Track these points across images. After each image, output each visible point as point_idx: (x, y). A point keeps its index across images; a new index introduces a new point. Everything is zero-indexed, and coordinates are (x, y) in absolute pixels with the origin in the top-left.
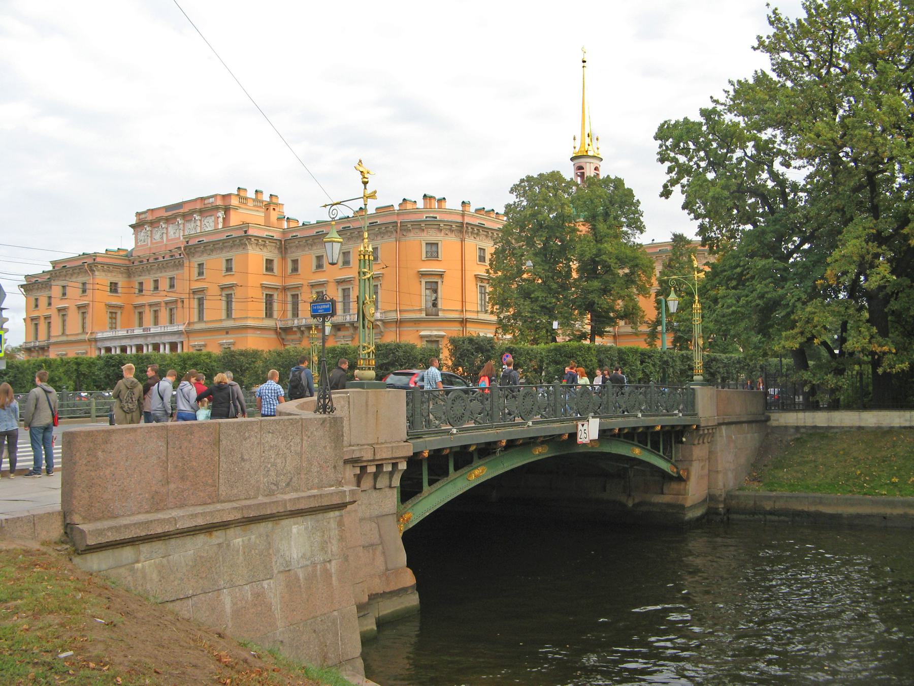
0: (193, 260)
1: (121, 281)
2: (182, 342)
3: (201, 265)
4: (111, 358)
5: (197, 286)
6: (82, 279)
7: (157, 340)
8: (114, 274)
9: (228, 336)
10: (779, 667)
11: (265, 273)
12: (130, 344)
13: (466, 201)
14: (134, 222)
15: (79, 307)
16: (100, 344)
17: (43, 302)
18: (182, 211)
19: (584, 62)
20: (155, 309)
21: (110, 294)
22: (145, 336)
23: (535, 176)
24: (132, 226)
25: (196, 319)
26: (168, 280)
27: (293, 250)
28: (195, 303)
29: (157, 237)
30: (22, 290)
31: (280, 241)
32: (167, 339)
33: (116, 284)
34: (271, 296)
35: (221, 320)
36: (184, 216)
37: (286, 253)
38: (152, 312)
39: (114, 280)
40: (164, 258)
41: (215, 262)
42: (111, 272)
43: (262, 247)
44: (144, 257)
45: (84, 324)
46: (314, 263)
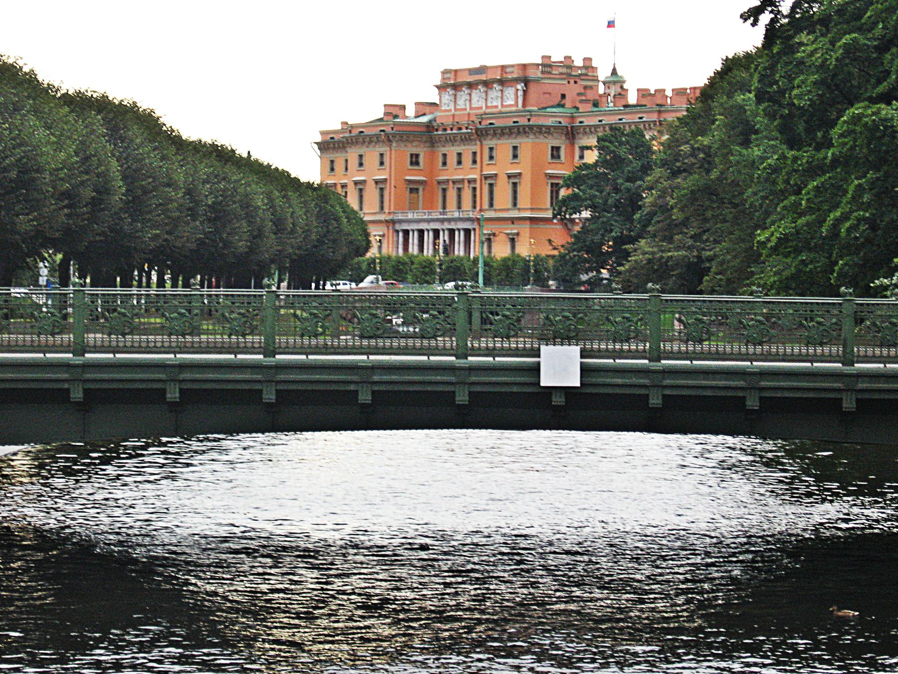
0: (485, 143)
1: (422, 151)
2: (474, 229)
3: (491, 149)
4: (452, 261)
7: (452, 226)
8: (414, 144)
9: (513, 226)
11: (550, 161)
12: (428, 227)
14: (439, 83)
15: (377, 182)
16: (398, 227)
17: (339, 166)
18: (483, 77)
20: (381, 186)
22: (442, 221)
23: (292, 176)
24: (437, 87)
25: (486, 205)
26: (511, 149)
27: (580, 136)
29: (461, 103)
30: (316, 147)
31: (567, 127)
32: (447, 226)
35: (508, 210)
36: (487, 84)
38: (511, 185)
39: (415, 151)
41: (504, 147)
42: (411, 142)
43: (546, 135)
44: (448, 125)
45: (382, 202)
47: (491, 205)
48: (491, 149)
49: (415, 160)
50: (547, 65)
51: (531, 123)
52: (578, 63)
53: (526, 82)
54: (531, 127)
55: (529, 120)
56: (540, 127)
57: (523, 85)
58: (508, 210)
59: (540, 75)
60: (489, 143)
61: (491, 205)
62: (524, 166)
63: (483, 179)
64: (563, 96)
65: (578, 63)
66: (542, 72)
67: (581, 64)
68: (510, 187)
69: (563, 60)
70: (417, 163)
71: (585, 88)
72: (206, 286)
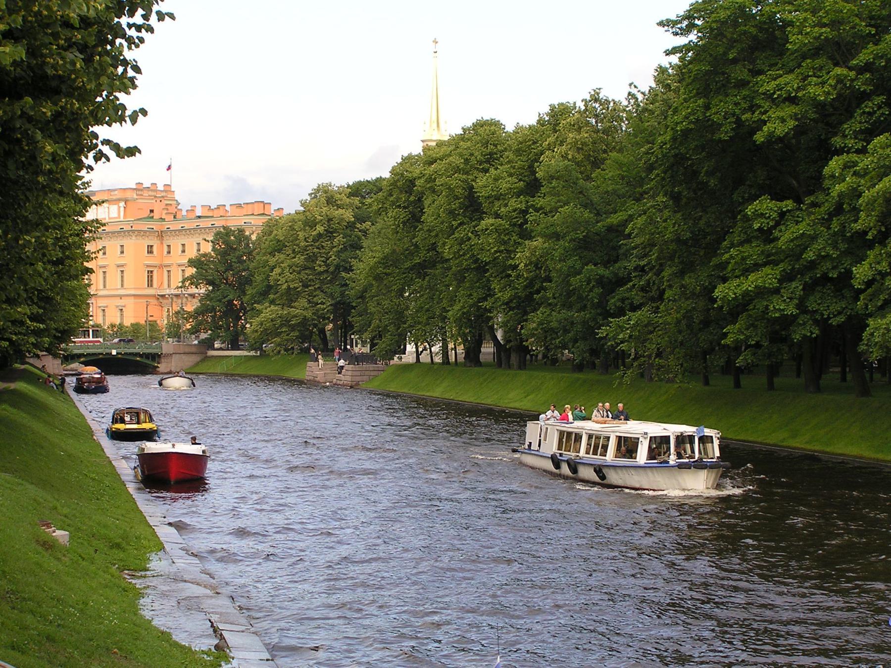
25: (101, 287)
34: (152, 272)
35: (117, 289)
37: (163, 240)
47: (105, 286)
50: (139, 189)
52: (160, 187)
53: (126, 201)
54: (133, 231)
56: (139, 231)
57: (124, 203)
58: (117, 289)
59: (135, 197)
61: (105, 286)
62: (128, 260)
64: (152, 211)
65: (160, 187)
66: (137, 195)
67: (162, 189)
68: (119, 273)
69: (149, 186)
71: (167, 205)
72: (591, 452)
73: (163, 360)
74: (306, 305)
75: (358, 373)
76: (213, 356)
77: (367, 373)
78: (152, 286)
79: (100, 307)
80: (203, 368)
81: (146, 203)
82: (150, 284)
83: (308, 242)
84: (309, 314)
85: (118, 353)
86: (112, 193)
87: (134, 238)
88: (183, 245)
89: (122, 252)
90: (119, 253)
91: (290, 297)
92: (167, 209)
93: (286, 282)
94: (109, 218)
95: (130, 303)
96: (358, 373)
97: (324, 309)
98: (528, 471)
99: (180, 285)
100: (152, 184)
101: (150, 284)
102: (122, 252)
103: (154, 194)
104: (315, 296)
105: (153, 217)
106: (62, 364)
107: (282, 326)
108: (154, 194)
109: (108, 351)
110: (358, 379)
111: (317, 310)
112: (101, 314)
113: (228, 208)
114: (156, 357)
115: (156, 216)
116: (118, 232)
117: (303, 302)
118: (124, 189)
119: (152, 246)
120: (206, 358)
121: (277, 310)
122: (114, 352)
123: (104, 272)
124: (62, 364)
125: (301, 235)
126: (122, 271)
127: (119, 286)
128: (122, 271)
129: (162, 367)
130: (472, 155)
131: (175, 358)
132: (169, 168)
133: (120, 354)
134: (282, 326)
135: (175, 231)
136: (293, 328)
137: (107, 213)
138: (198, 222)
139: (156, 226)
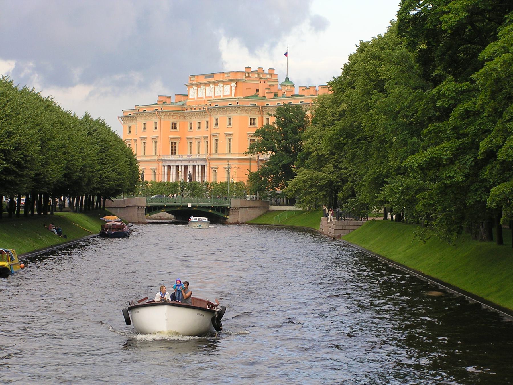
5: (214, 132)
6: (155, 119)
10: (208, 220)
12: (181, 164)
13: (285, 52)
15: (153, 138)
19: (286, 54)
21: (172, 130)
22: (189, 160)
25: (213, 151)
28: (214, 142)
33: (176, 124)
35: (226, 154)
37: (263, 114)
39: (174, 121)
40: (195, 109)
41: (223, 118)
46: (227, 122)
47: (216, 151)
48: (217, 119)
49: (174, 126)
51: (238, 105)
54: (239, 107)
55: (238, 103)
56: (244, 107)
57: (235, 84)
59: (244, 78)
60: (214, 116)
62: (234, 129)
63: (212, 136)
66: (246, 77)
70: (175, 128)
71: (270, 85)
73: (231, 213)
74: (332, 169)
75: (340, 227)
76: (273, 211)
77: (348, 227)
78: (175, 154)
79: (212, 168)
80: (264, 220)
81: (253, 84)
82: (173, 152)
83: (334, 117)
84: (333, 177)
85: (192, 206)
86: (226, 75)
87: (239, 112)
88: (230, 119)
89: (230, 124)
90: (228, 124)
91: (321, 161)
92: (269, 89)
93: (316, 150)
94: (223, 96)
95: (235, 164)
96: (340, 227)
97: (346, 173)
98: (157, 348)
99: (248, 150)
100: (259, 68)
101: (173, 152)
102: (230, 124)
103: (260, 76)
104: (340, 163)
105: (258, 96)
106: (145, 214)
107: (311, 186)
108: (260, 76)
109: (184, 204)
110: (341, 232)
111: (341, 174)
112: (212, 174)
113: (317, 88)
114: (226, 210)
115: (260, 94)
116: (227, 107)
117: (329, 167)
118: (236, 72)
119: (254, 119)
120: (268, 212)
121: (308, 173)
122: (190, 205)
123: (216, 140)
124: (145, 214)
125: (329, 111)
126: (230, 139)
127: (227, 152)
128: (230, 139)
129: (230, 218)
130: (386, 44)
131: (241, 211)
132: (286, 54)
133: (195, 207)
134: (311, 186)
135: (223, 108)
136: (321, 188)
137: (222, 92)
138: (290, 100)
139: (258, 103)
